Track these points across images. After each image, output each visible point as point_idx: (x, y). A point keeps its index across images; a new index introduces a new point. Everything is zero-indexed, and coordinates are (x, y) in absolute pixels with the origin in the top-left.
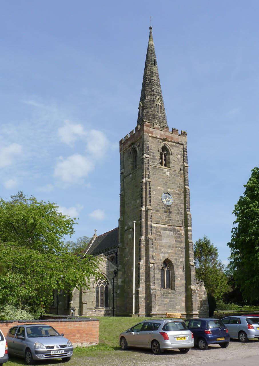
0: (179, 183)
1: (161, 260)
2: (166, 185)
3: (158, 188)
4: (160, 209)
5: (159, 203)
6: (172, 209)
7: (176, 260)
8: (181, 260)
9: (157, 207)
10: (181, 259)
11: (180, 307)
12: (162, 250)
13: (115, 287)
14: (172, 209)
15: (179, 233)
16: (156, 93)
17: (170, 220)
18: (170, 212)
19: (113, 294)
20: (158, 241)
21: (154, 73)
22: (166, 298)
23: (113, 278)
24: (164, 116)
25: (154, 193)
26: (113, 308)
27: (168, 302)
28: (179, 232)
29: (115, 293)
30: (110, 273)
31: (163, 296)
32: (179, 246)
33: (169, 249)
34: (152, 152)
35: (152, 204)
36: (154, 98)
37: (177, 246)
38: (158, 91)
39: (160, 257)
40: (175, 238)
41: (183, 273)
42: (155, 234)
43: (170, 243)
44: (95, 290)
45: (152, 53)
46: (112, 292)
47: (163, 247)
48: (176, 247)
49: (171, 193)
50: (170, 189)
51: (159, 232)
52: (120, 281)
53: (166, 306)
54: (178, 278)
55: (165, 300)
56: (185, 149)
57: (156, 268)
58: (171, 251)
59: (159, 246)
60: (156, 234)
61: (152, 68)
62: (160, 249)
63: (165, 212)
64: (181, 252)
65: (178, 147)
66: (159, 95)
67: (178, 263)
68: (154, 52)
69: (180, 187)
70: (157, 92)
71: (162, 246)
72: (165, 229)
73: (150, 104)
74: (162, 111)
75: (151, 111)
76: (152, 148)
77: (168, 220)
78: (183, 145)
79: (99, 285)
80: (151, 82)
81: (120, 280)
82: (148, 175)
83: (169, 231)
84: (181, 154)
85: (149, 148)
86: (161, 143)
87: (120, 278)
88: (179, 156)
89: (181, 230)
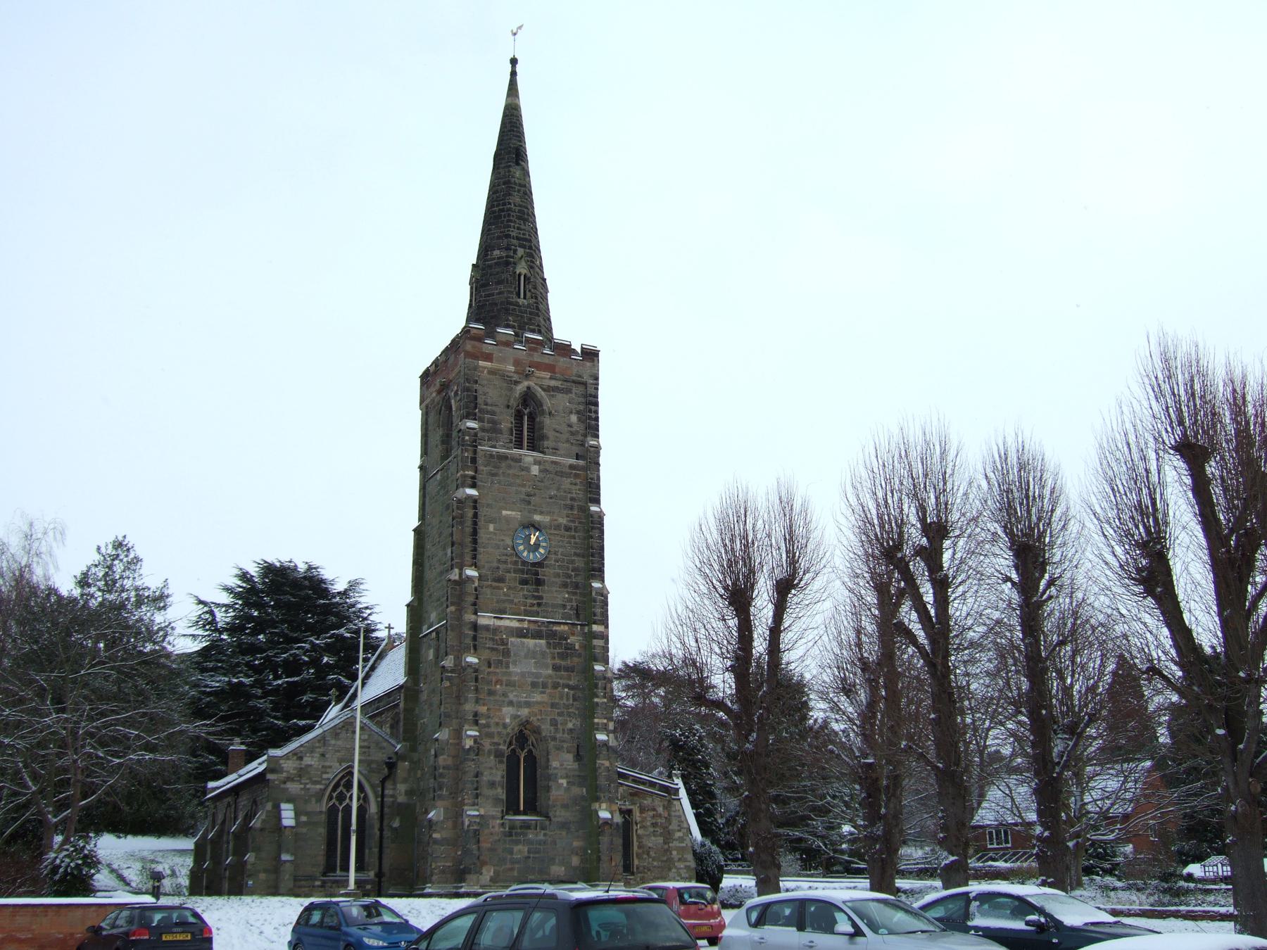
0: (569, 495)
1: (505, 726)
2: (529, 503)
3: (504, 512)
4: (508, 575)
5: (504, 557)
6: (546, 573)
7: (556, 725)
8: (570, 725)
9: (498, 568)
10: (571, 721)
11: (563, 869)
12: (511, 696)
13: (386, 810)
14: (547, 574)
15: (567, 643)
16: (515, 242)
17: (539, 605)
18: (539, 583)
19: (381, 830)
20: (498, 671)
21: (515, 184)
22: (518, 842)
23: (383, 782)
24: (536, 303)
25: (491, 527)
26: (380, 875)
27: (526, 854)
28: (566, 639)
29: (386, 828)
30: (374, 766)
31: (510, 835)
32: (565, 682)
33: (533, 692)
34: (488, 412)
35: (482, 558)
36: (507, 257)
37: (558, 683)
38: (523, 234)
39: (504, 719)
40: (554, 658)
41: (577, 763)
42: (489, 648)
43: (537, 675)
44: (323, 817)
45: (513, 131)
46: (377, 826)
47: (514, 686)
48: (555, 686)
49: (545, 527)
50: (541, 513)
51: (504, 642)
52: (403, 791)
53: (517, 866)
54: (561, 781)
55: (516, 848)
56: (591, 396)
57: (490, 752)
58: (537, 697)
59: (501, 685)
60: (492, 649)
61: (509, 171)
62: (505, 695)
63: (524, 582)
64: (571, 702)
65: (571, 393)
66: (523, 246)
67: (561, 735)
68: (517, 127)
69: (572, 508)
70: (518, 238)
71: (510, 684)
72: (521, 633)
73: (498, 273)
74: (530, 291)
75: (500, 293)
76: (489, 401)
77: (532, 605)
78: (585, 384)
79: (337, 804)
80: (502, 210)
81: (402, 788)
82: (473, 478)
83: (533, 637)
84: (578, 412)
85: (480, 401)
86: (519, 382)
87: (402, 782)
88: (574, 418)
89: (573, 634)
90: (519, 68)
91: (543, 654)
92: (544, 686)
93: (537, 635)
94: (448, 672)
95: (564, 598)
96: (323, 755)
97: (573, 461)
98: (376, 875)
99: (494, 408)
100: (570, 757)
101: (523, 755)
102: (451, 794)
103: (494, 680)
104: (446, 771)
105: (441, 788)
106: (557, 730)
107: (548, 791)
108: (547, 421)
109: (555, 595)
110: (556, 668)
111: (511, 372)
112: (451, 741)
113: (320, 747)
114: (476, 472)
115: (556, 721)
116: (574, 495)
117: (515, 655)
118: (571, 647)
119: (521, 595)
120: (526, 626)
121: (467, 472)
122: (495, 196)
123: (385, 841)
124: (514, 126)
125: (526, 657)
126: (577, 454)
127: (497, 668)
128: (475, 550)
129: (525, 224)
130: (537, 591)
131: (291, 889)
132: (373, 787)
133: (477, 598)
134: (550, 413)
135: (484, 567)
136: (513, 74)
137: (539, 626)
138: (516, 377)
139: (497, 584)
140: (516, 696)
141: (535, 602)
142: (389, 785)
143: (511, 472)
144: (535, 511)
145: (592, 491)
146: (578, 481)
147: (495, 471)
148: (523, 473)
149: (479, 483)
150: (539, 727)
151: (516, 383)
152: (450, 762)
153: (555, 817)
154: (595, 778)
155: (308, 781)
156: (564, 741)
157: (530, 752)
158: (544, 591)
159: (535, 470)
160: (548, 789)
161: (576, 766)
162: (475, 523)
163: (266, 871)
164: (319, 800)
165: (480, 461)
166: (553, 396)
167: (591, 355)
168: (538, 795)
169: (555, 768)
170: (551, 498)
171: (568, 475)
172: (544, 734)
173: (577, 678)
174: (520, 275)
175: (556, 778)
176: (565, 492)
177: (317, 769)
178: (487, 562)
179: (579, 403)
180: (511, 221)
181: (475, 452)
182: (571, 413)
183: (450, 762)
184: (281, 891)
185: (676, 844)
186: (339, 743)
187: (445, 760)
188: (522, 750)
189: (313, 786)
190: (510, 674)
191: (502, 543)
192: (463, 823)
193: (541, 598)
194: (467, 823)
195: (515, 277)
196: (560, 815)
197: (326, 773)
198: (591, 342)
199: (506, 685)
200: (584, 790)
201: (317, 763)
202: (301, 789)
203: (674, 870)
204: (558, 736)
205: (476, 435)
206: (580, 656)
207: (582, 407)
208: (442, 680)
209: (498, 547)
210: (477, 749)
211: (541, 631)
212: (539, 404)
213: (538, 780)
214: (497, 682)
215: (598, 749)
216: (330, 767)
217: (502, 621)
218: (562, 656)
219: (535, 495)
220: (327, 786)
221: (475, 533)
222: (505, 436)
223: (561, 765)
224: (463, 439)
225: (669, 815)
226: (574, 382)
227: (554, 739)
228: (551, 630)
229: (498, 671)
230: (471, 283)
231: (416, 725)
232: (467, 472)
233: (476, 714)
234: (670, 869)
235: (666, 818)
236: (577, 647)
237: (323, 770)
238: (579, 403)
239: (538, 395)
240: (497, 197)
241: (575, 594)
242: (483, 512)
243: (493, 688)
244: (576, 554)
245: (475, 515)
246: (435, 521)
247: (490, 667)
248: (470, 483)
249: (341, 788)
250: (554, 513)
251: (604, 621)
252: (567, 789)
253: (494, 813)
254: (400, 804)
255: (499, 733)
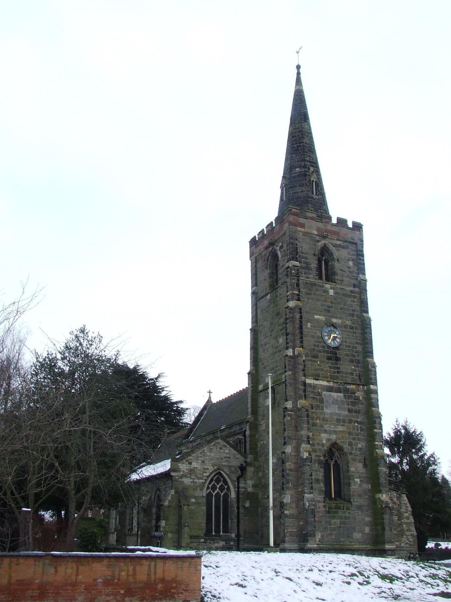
1: (323, 445)
2: (329, 311)
3: (316, 317)
4: (320, 354)
8: (360, 446)
10: (360, 443)
12: (326, 427)
13: (241, 496)
16: (308, 163)
18: (338, 359)
19: (238, 508)
20: (317, 411)
21: (305, 132)
22: (334, 518)
25: (309, 325)
26: (238, 536)
27: (339, 525)
29: (241, 507)
30: (233, 469)
31: (329, 512)
33: (338, 425)
34: (303, 258)
36: (305, 171)
37: (352, 420)
39: (322, 441)
40: (348, 405)
42: (311, 397)
43: (339, 415)
44: (204, 500)
46: (235, 505)
47: (327, 421)
48: (350, 421)
49: (339, 327)
50: (336, 318)
51: (320, 394)
52: (251, 485)
54: (356, 480)
55: (333, 521)
58: (340, 428)
59: (320, 420)
60: (314, 398)
62: (322, 426)
63: (329, 358)
64: (360, 432)
65: (349, 249)
66: (313, 166)
69: (353, 315)
70: (310, 162)
71: (324, 420)
72: (330, 389)
75: (301, 192)
76: (304, 251)
78: (356, 244)
80: (300, 146)
81: (250, 483)
82: (298, 295)
83: (336, 392)
84: (353, 260)
88: (351, 263)
89: (358, 391)
90: (301, 71)
91: (342, 401)
92: (344, 421)
93: (338, 391)
94: (289, 411)
95: (352, 369)
96: (203, 462)
97: (351, 288)
98: (236, 536)
99: (307, 255)
100: (360, 465)
101: (332, 463)
102: (294, 486)
103: (315, 417)
104: (290, 472)
105: (288, 483)
106: (352, 448)
107: (349, 486)
108: (336, 264)
109: (347, 367)
110: (350, 411)
111: (315, 235)
112: (292, 454)
113: (201, 457)
114: (299, 292)
115: (352, 443)
116: (354, 308)
117: (326, 402)
118: (357, 398)
119: (327, 366)
120: (331, 385)
121: (294, 292)
122: (294, 138)
123: (241, 515)
124: (301, 101)
125: (333, 403)
126: (354, 284)
127: (316, 409)
128: (302, 338)
129: (312, 154)
130: (337, 364)
131: (188, 544)
132: (232, 482)
133: (305, 367)
134: (338, 260)
135: (306, 348)
136: (299, 74)
137: (339, 385)
138: (318, 238)
139: (314, 359)
140: (329, 427)
141: (336, 370)
142: (242, 481)
143: (318, 293)
144: (333, 317)
145: (363, 305)
146: (356, 300)
147: (309, 292)
148: (325, 294)
149: (301, 299)
150: (342, 446)
151: (318, 241)
152: (293, 466)
153: (354, 502)
154: (378, 479)
155: (195, 477)
156: (356, 456)
157: (336, 461)
158: (340, 364)
159: (331, 292)
160: (349, 485)
161: (364, 470)
162: (301, 322)
163: (171, 532)
164: (202, 489)
165: (301, 286)
166: (338, 250)
167: (358, 227)
168: (342, 488)
169: (353, 472)
170: (341, 309)
171: (350, 296)
172: (345, 451)
173: (362, 417)
174: (313, 181)
175: (353, 478)
176: (349, 306)
177: (200, 470)
178: (308, 346)
179: (353, 255)
180: (305, 152)
181: (298, 280)
182: (349, 260)
183: (293, 466)
184: (183, 545)
185: (405, 520)
186: (212, 455)
187: (289, 465)
188: (332, 461)
189: (198, 480)
190: (324, 413)
191: (315, 334)
192: (304, 504)
193: (339, 368)
194: (307, 504)
195: (310, 183)
196: (357, 501)
197: (206, 473)
198: (79, 326)
199: (322, 420)
200: (370, 486)
201: (200, 466)
202: (191, 482)
203: (405, 536)
204: (353, 452)
205: (298, 270)
206: (362, 404)
207: (354, 257)
208: (285, 416)
209: (313, 337)
210: (310, 459)
211: (340, 388)
212: (331, 254)
213: (342, 479)
214: (317, 419)
215: (379, 460)
216: (208, 469)
217: (318, 381)
218: (353, 404)
219: (332, 307)
220: (206, 480)
221: (301, 328)
222: (314, 272)
223: (356, 470)
224: (291, 272)
225: (400, 503)
226: (350, 242)
227: (351, 454)
228: (346, 388)
229: (317, 411)
230: (282, 187)
231: (257, 445)
232: (294, 292)
233: (308, 437)
234: (402, 536)
235: (399, 505)
236: (361, 399)
237: (204, 471)
238: (353, 255)
239: (331, 249)
240: (295, 139)
241: (357, 366)
242: (305, 315)
243: (315, 422)
244: (357, 343)
245: (301, 317)
246: (267, 324)
247: (312, 408)
248: (297, 298)
249: (214, 482)
250: (343, 318)
251: (375, 384)
252: (360, 485)
253: (320, 499)
254: (249, 493)
255: (320, 450)
